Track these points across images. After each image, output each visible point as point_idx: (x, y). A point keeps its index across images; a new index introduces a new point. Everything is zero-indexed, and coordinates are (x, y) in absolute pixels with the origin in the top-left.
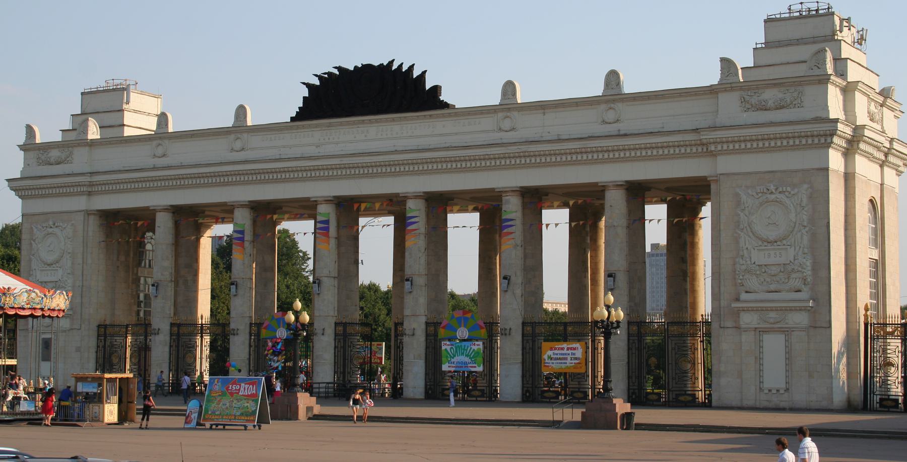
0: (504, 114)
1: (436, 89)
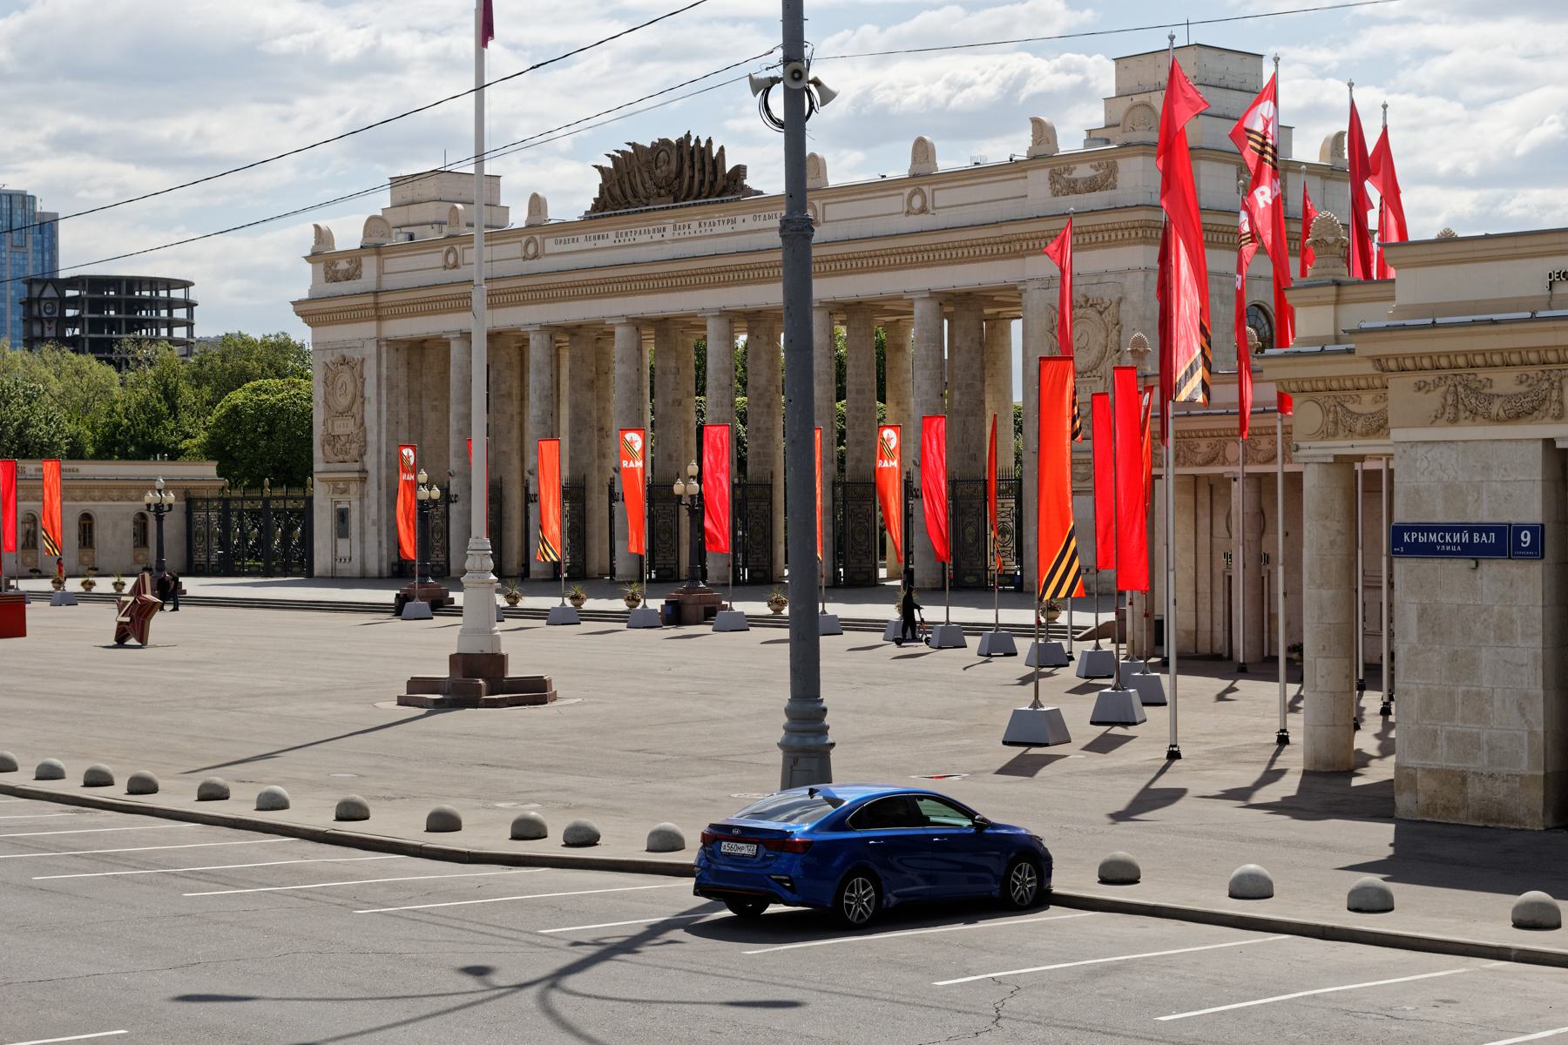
0: (1056, 323)
1: (740, 171)
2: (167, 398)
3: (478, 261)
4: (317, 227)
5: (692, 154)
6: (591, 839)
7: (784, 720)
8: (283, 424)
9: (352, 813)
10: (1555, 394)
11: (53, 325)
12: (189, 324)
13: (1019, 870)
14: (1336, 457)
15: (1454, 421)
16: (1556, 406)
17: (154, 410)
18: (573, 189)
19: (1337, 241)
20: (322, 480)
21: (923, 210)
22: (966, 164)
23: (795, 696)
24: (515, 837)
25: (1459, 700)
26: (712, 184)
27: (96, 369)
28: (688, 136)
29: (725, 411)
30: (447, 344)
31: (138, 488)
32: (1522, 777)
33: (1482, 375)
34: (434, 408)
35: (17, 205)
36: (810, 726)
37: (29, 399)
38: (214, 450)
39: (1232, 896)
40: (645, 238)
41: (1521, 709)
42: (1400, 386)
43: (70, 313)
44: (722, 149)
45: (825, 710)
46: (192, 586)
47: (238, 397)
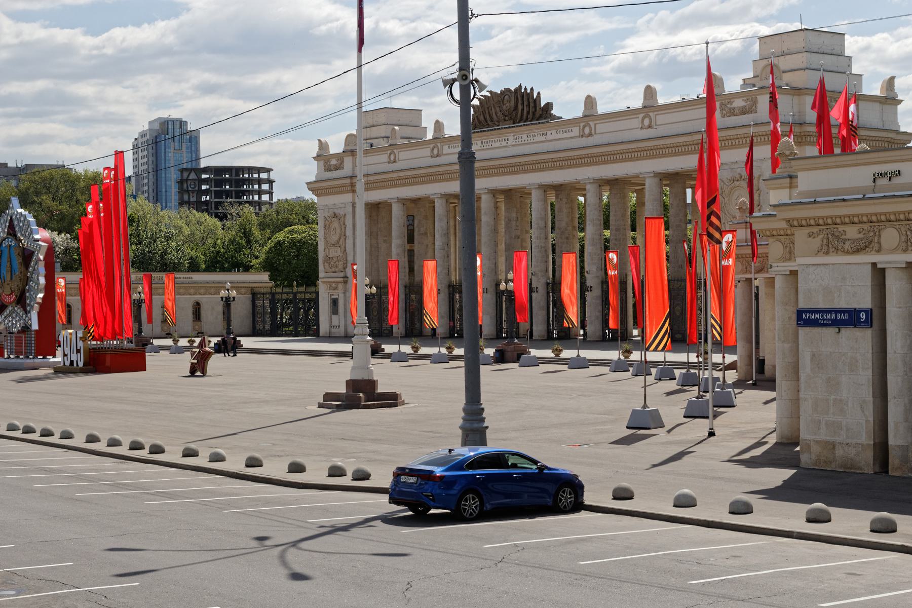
1: (549, 106)
2: (245, 236)
3: (408, 159)
4: (320, 141)
5: (523, 96)
6: (366, 476)
7: (463, 414)
8: (306, 251)
9: (254, 463)
10: (876, 239)
11: (195, 194)
12: (270, 193)
13: (564, 492)
14: (791, 271)
15: (827, 253)
16: (876, 245)
17: (239, 244)
19: (791, 153)
20: (323, 283)
21: (650, 127)
22: (678, 99)
23: (467, 403)
24: (330, 476)
25: (831, 403)
26: (534, 113)
27: (211, 221)
28: (520, 86)
29: (502, 243)
30: (390, 205)
31: (216, 288)
32: (863, 445)
33: (841, 228)
34: (385, 241)
35: (177, 126)
36: (475, 418)
37: (168, 238)
38: (268, 266)
39: (675, 506)
40: (498, 144)
41: (862, 408)
42: (800, 235)
43: (204, 187)
44: (539, 93)
45: (483, 409)
46: (247, 342)
47: (281, 236)
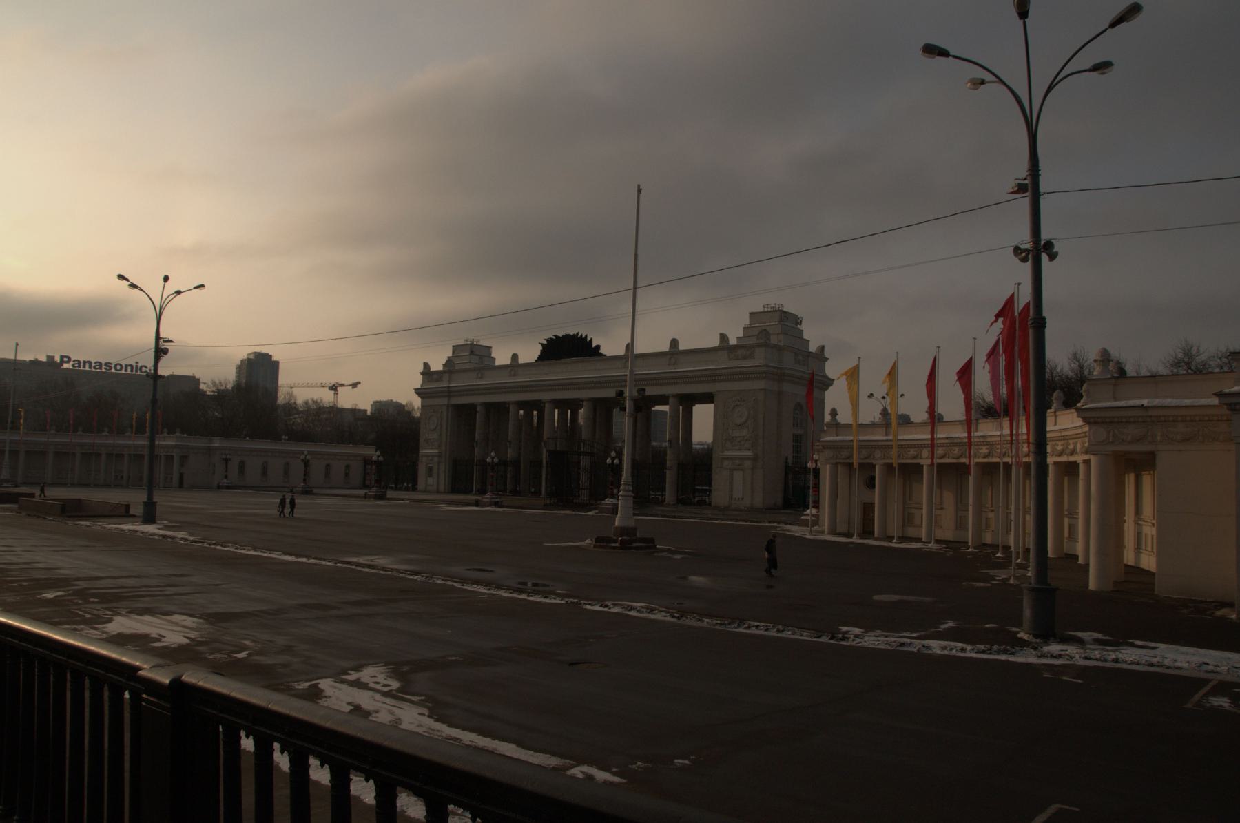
1: (598, 347)
18: (530, 353)
